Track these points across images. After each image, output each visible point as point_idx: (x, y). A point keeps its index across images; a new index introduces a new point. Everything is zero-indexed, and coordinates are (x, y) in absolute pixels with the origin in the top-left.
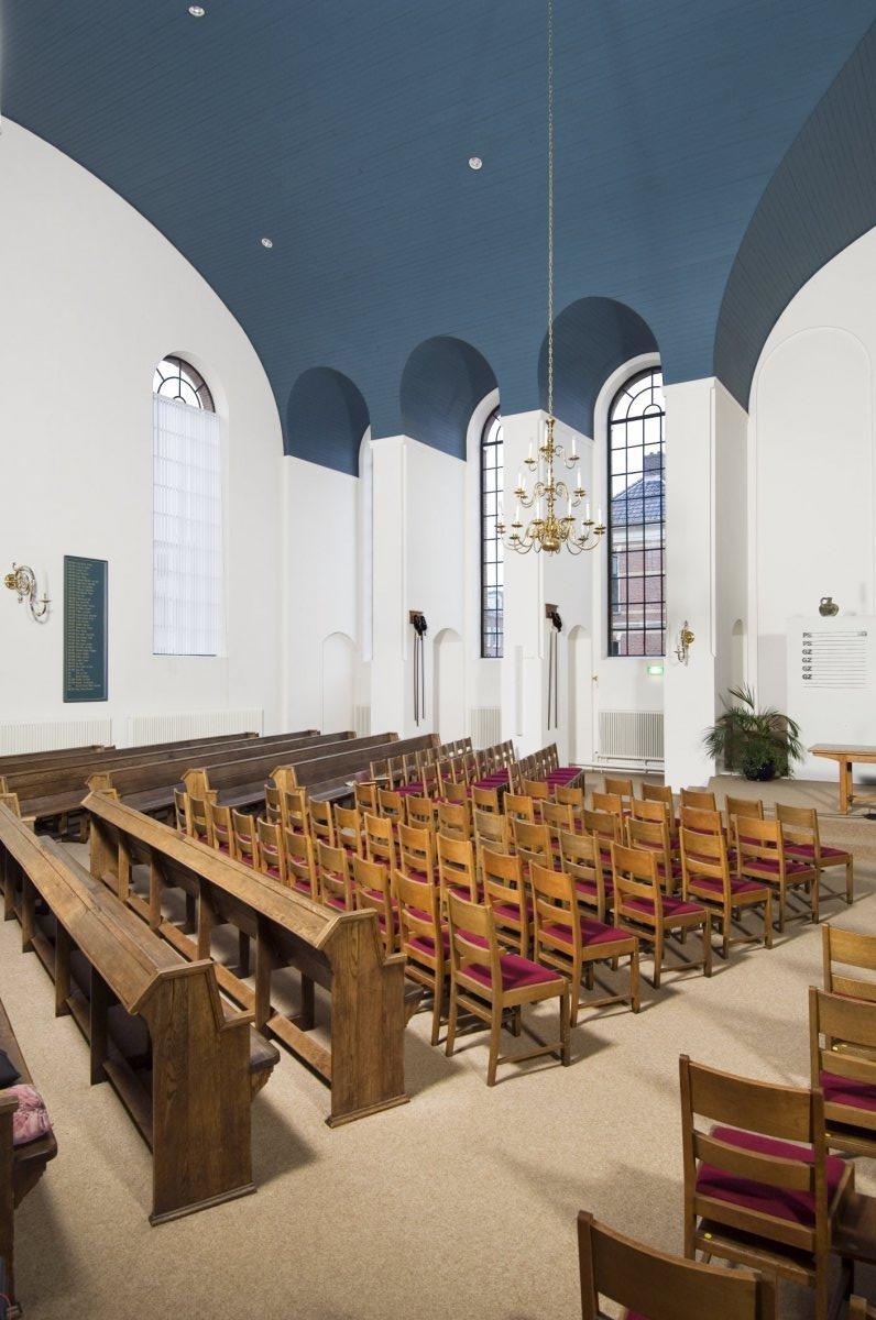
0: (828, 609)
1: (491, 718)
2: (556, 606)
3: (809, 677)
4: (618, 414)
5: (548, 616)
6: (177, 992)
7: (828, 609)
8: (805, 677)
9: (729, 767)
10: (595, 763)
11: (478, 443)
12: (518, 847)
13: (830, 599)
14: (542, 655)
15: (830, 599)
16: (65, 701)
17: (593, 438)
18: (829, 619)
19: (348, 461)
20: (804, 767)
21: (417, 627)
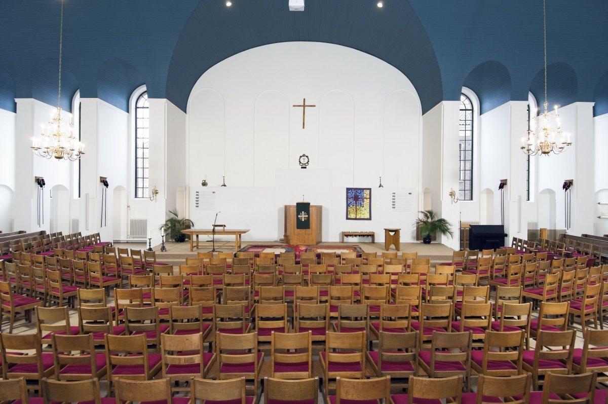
0: (204, 184)
1: (75, 223)
2: (106, 178)
3: (394, 208)
4: (140, 104)
5: (101, 181)
6: (532, 384)
7: (204, 184)
8: (393, 208)
9: (418, 239)
10: (128, 239)
11: (134, 107)
12: (151, 274)
13: (205, 181)
14: (166, 197)
15: (205, 181)
16: (528, 223)
17: (186, 113)
18: (204, 187)
19: (125, 106)
20: (509, 242)
21: (39, 183)
